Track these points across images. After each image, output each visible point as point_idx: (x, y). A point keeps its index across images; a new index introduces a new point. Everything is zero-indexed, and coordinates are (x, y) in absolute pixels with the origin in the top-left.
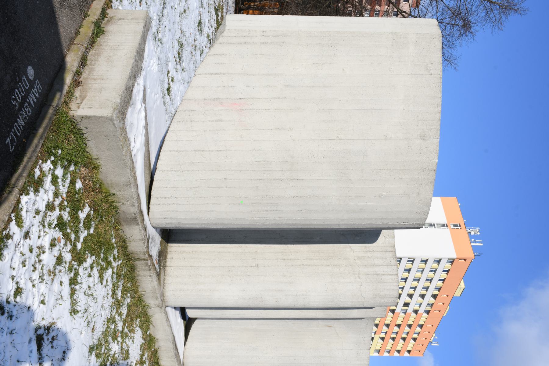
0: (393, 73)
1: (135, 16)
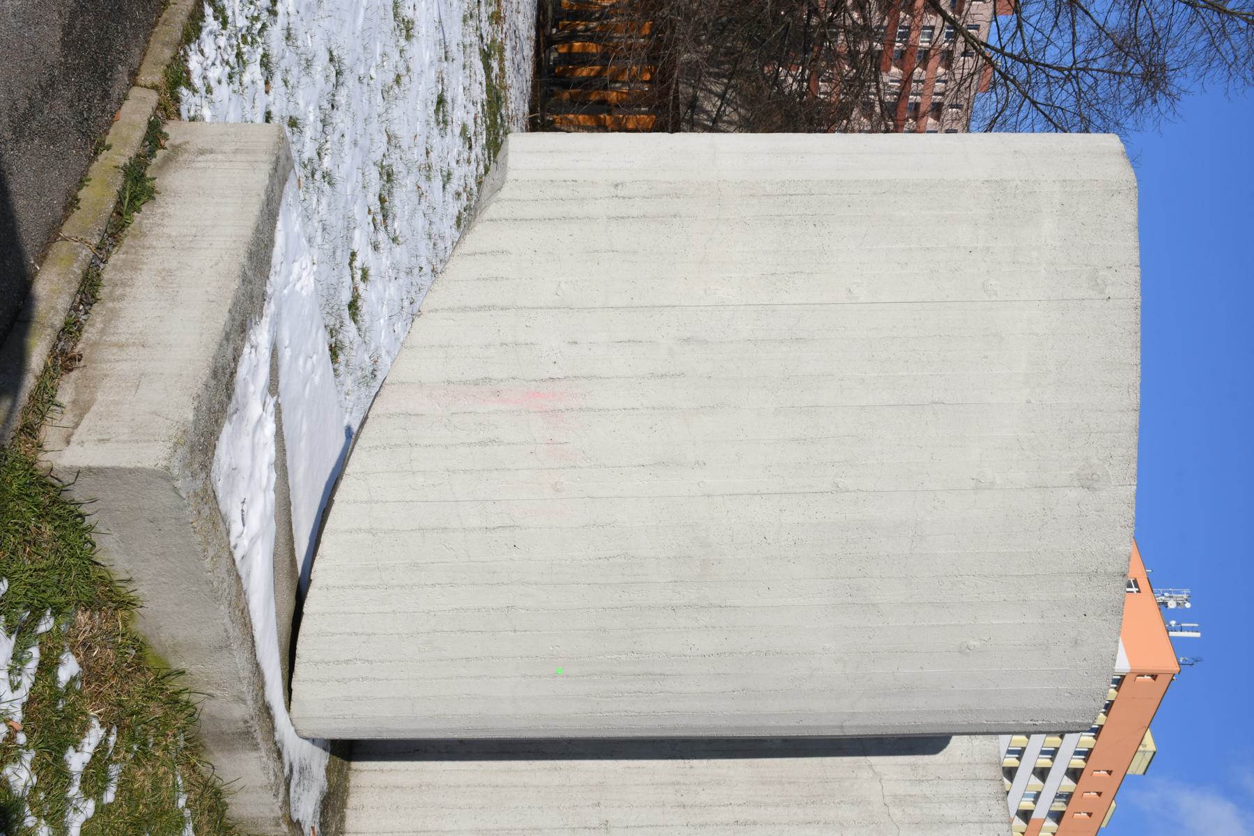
0: (994, 298)
1: (247, 142)
